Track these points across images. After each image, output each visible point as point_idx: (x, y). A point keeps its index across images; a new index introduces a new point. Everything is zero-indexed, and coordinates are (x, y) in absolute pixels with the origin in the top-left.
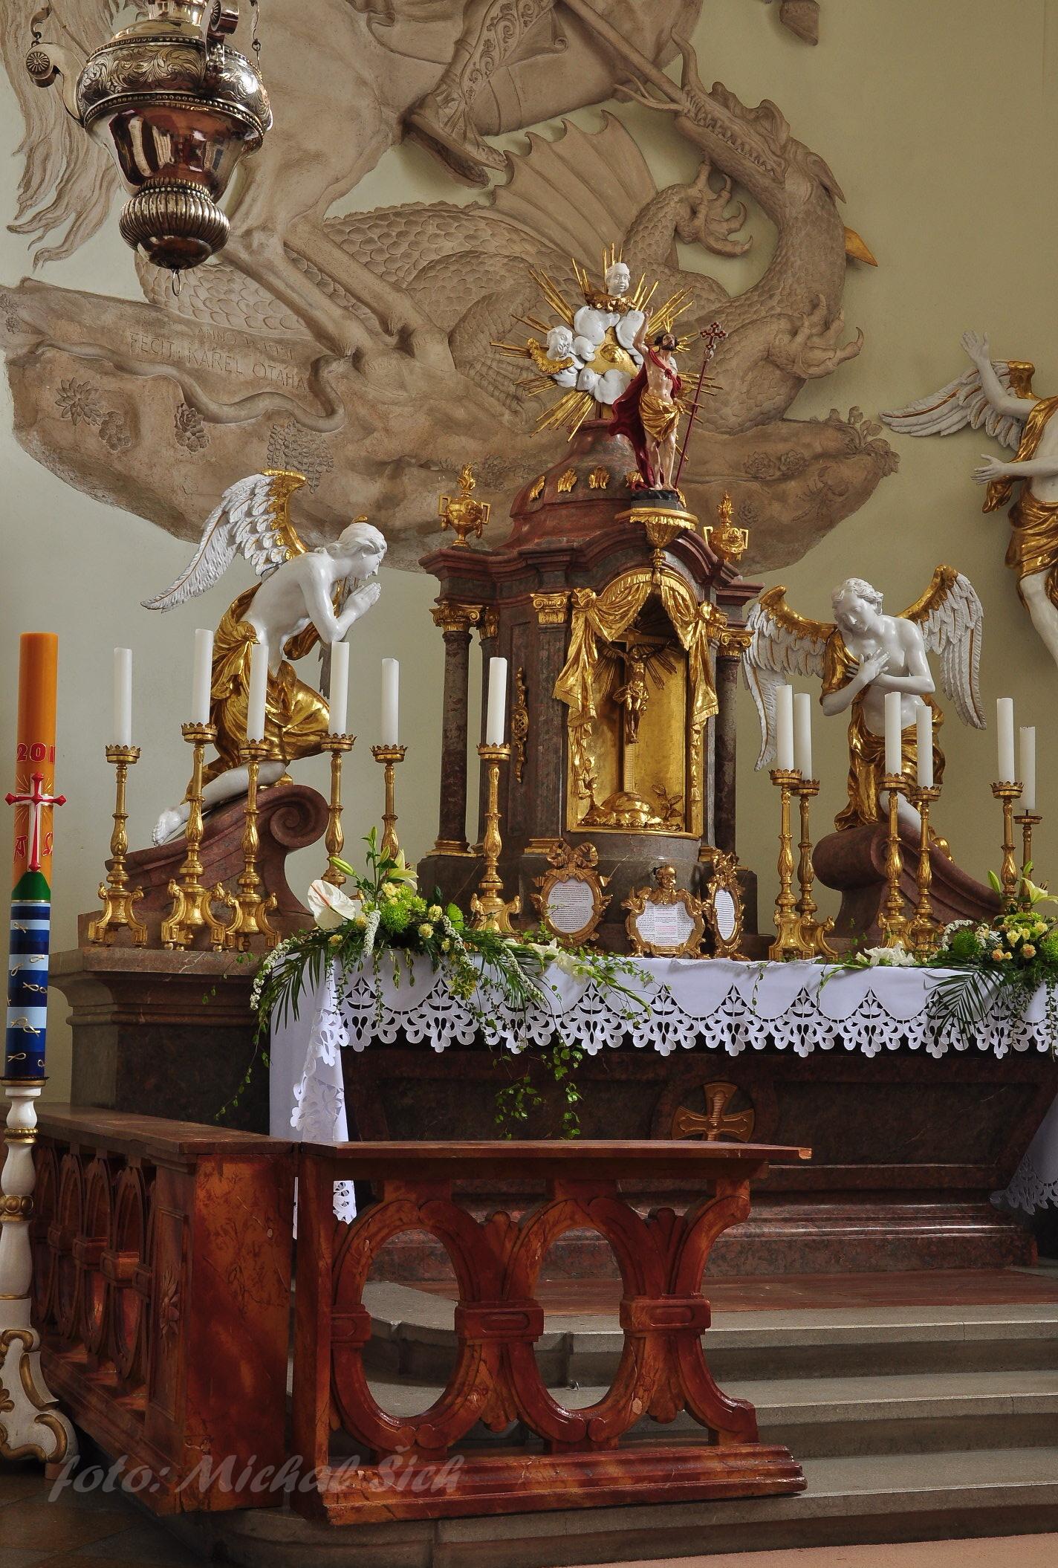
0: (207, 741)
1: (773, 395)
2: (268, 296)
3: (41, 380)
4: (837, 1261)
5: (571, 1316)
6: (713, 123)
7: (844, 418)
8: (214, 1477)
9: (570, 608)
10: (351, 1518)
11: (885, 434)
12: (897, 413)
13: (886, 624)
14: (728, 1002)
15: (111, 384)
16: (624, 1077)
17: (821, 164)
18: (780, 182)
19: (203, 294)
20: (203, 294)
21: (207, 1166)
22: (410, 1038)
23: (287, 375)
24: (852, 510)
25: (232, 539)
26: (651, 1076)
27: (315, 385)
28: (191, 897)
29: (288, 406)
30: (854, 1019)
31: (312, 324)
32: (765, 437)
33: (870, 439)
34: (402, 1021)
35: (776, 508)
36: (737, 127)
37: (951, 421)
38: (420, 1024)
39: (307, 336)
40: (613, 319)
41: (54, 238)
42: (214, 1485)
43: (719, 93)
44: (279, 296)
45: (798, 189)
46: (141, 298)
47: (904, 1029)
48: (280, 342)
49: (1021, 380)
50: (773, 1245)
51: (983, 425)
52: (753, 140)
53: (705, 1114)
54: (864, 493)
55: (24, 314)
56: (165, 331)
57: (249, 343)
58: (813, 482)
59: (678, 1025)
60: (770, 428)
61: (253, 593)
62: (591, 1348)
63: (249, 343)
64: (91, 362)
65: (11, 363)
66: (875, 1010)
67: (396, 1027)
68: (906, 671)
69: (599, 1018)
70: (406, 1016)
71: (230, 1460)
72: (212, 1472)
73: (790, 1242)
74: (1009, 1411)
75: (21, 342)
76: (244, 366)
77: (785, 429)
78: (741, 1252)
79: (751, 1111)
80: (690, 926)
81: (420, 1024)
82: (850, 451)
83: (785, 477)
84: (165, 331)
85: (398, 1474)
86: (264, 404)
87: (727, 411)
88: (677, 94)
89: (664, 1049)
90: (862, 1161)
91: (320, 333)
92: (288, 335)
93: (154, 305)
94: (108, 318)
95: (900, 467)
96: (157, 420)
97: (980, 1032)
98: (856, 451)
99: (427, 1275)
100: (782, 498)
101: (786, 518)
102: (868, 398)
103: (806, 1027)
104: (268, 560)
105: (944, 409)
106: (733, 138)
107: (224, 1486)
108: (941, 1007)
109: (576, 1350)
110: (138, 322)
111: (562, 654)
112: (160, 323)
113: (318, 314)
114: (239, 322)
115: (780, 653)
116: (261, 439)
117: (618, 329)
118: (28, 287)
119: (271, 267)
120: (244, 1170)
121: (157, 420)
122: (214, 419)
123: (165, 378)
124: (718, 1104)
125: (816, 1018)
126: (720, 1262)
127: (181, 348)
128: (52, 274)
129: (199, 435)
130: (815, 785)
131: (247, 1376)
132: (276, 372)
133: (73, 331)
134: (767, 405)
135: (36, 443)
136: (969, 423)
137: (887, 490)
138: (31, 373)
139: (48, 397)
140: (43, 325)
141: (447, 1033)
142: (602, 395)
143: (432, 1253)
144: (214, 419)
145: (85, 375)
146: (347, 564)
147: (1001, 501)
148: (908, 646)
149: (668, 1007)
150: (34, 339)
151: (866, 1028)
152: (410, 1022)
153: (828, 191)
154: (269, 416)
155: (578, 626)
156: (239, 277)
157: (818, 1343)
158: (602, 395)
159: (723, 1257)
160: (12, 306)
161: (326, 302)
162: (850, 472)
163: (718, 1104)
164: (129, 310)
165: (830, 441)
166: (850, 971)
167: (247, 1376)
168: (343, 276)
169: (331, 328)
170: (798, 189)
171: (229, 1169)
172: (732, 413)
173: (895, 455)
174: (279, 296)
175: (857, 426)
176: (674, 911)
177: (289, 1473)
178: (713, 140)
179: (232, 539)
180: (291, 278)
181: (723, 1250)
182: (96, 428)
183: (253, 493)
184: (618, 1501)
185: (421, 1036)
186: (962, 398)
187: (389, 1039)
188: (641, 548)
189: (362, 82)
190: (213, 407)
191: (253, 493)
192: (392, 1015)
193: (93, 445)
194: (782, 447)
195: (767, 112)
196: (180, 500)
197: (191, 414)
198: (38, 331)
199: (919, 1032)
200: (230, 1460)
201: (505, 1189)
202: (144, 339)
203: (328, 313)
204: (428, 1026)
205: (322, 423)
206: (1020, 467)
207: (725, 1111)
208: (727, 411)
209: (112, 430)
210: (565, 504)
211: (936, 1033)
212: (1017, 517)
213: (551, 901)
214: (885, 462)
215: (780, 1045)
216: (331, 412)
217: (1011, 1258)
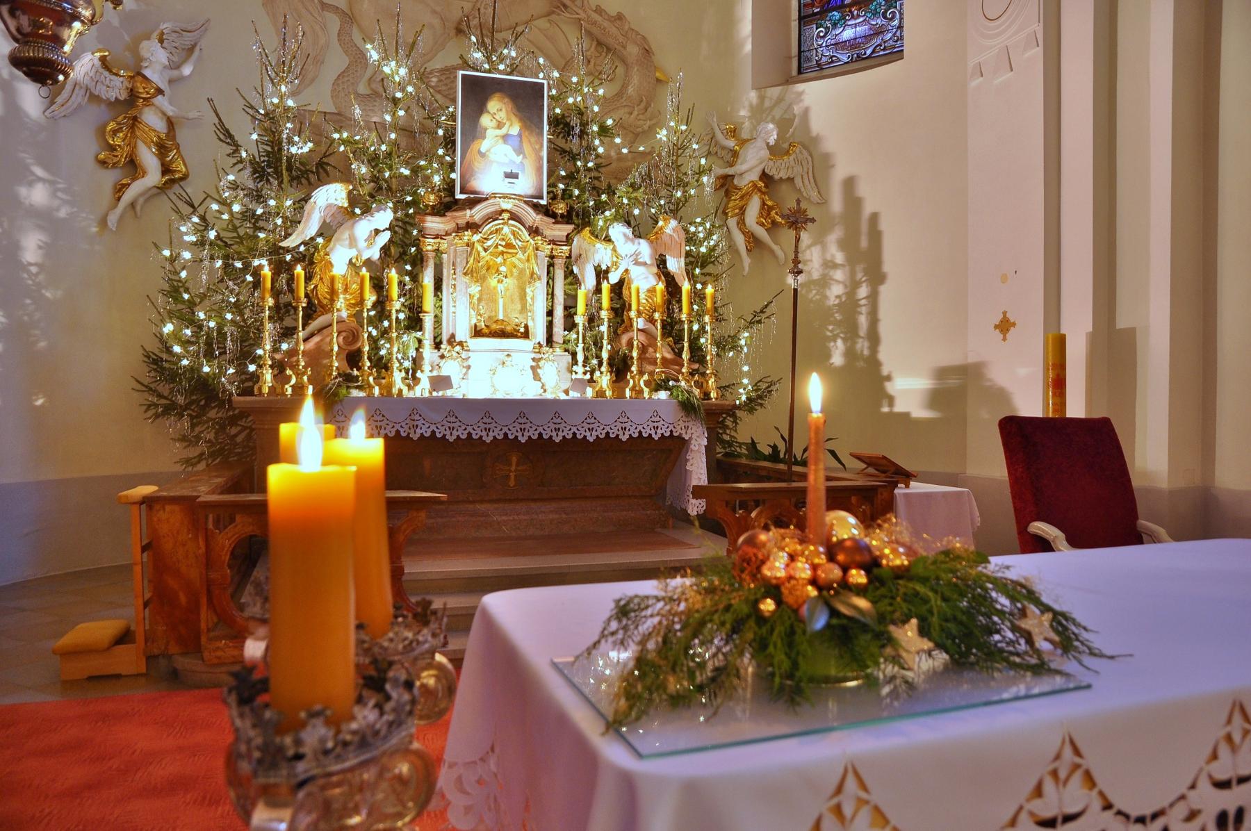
6: (595, 23)
10: (216, 661)
17: (644, 38)
18: (624, 47)
21: (157, 507)
22: (474, 437)
36: (606, 24)
38: (582, 431)
43: (599, 10)
45: (633, 50)
52: (614, 30)
66: (417, 417)
69: (527, 426)
81: (514, 430)
88: (580, 11)
106: (604, 29)
113: (164, 109)
120: (176, 508)
124: (514, 460)
131: (183, 598)
147: (722, 186)
149: (453, 419)
153: (647, 52)
167: (183, 598)
170: (633, 50)
171: (168, 508)
178: (595, 30)
187: (464, 437)
189: (434, 12)
195: (620, 17)
206: (730, 171)
207: (517, 465)
212: (728, 194)
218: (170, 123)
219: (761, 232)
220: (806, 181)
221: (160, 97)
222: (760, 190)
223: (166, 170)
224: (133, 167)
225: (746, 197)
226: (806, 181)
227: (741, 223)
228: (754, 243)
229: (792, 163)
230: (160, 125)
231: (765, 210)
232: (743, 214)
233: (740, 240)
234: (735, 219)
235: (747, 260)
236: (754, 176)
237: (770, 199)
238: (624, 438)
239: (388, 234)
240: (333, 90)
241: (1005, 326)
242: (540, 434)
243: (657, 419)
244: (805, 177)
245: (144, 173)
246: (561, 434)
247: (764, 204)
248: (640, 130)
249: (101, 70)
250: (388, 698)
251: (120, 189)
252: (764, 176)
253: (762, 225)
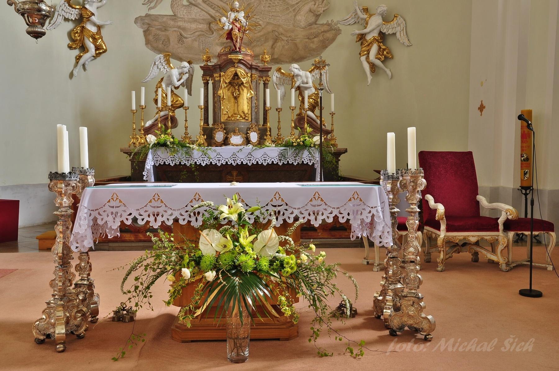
1: (312, 19)
2: (199, 10)
3: (149, 34)
9: (220, 76)
11: (339, 25)
13: (302, 73)
14: (153, 200)
15: (163, 33)
19: (185, 11)
20: (185, 11)
22: (166, 163)
23: (204, 26)
24: (331, 43)
25: (158, 68)
27: (210, 28)
28: (141, 138)
29: (203, 33)
30: (145, 209)
31: (209, 14)
32: (311, 29)
34: (165, 160)
35: (311, 45)
37: (352, 21)
39: (209, 17)
41: (152, 5)
42: (446, 349)
44: (202, 10)
46: (173, 14)
47: (273, 160)
48: (203, 19)
49: (366, 10)
54: (333, 39)
55: (146, 21)
57: (195, 21)
58: (321, 38)
59: (285, 211)
60: (312, 26)
63: (195, 21)
64: (160, 29)
65: (144, 31)
67: (333, 215)
68: (307, 83)
70: (97, 211)
71: (452, 340)
75: (146, 27)
76: (194, 26)
77: (316, 26)
80: (242, 140)
82: (331, 29)
83: (315, 37)
85: (511, 344)
86: (197, 33)
87: (301, 24)
89: (219, 165)
91: (212, 17)
92: (205, 18)
93: (175, 15)
94: (165, 19)
95: (342, 32)
96: (173, 39)
97: (182, 215)
100: (313, 42)
101: (314, 47)
102: (335, 17)
103: (279, 212)
105: (350, 19)
107: (450, 349)
108: (282, 155)
112: (176, 19)
113: (210, 13)
114: (193, 16)
115: (282, 80)
116: (196, 41)
118: (147, 16)
119: (199, 4)
121: (173, 39)
122: (186, 38)
123: (175, 31)
125: (123, 208)
127: (180, 24)
128: (152, 12)
129: (183, 41)
130: (281, 109)
132: (201, 26)
133: (157, 23)
134: (310, 22)
135: (150, 47)
137: (339, 39)
138: (147, 33)
139: (151, 38)
140: (150, 23)
141: (220, 162)
144: (186, 38)
145: (158, 32)
146: (180, 71)
148: (307, 78)
150: (148, 26)
151: (112, 213)
152: (99, 214)
154: (199, 36)
155: (222, 80)
156: (193, 7)
160: (144, 20)
161: (212, 10)
162: (329, 35)
164: (169, 17)
165: (326, 28)
166: (260, 148)
168: (216, 4)
169: (213, 15)
172: (303, 24)
174: (202, 10)
176: (239, 137)
177: (472, 345)
179: (158, 68)
180: (204, 6)
182: (161, 43)
183: (160, 58)
184: (141, 241)
185: (145, 221)
187: (162, 164)
188: (231, 63)
190: (185, 35)
191: (160, 58)
192: (370, 209)
193: (161, 46)
194: (315, 31)
196: (180, 55)
197: (181, 38)
198: (149, 24)
199: (276, 160)
200: (452, 340)
202: (172, 23)
203: (212, 12)
204: (149, 216)
205: (210, 36)
207: (237, 176)
208: (301, 24)
209: (164, 43)
211: (280, 160)
213: (216, 136)
214: (338, 32)
215: (244, 163)
216: (213, 33)
218: (99, 27)
219: (378, 62)
220: (402, 35)
221: (93, 17)
222: (377, 41)
223: (97, 48)
224: (84, 49)
225: (370, 44)
226: (402, 35)
227: (367, 58)
228: (373, 67)
229: (395, 25)
230: (93, 29)
231: (380, 51)
232: (369, 54)
233: (367, 67)
234: (365, 57)
235: (370, 77)
236: (375, 34)
237: (384, 45)
238: (219, 165)
239: (187, 75)
240: (172, 4)
241: (482, 108)
242: (242, 162)
243: (266, 156)
244: (402, 32)
245: (88, 51)
246: (266, 162)
247: (380, 48)
248: (319, 13)
249: (68, 7)
250: (297, 300)
251: (78, 58)
252: (381, 34)
253: (379, 59)
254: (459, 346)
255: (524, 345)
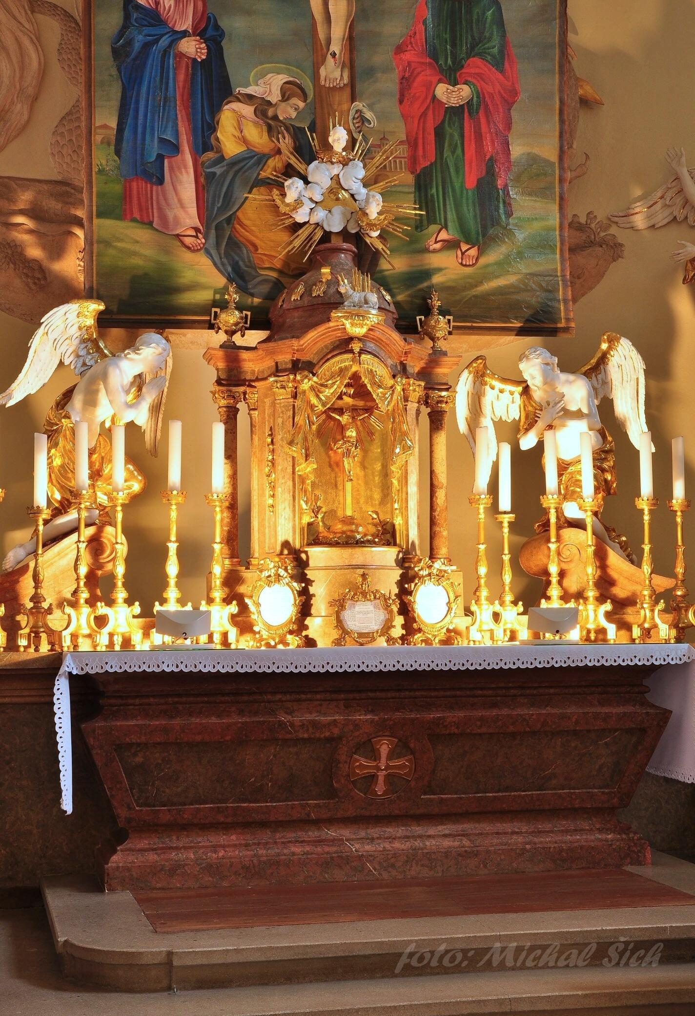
0: (569, 414)
4: (485, 866)
5: (197, 930)
7: (583, 220)
8: (502, 957)
11: (613, 230)
12: (621, 214)
16: (306, 736)
26: (327, 734)
33: (602, 234)
40: (336, 170)
50: (433, 856)
51: (686, 218)
53: (375, 760)
56: (71, 200)
61: (75, 386)
62: (189, 962)
72: (504, 958)
73: (446, 853)
74: (507, 1009)
78: (407, 862)
79: (410, 757)
84: (71, 200)
90: (506, 789)
98: (591, 244)
99: (159, 885)
104: (84, 364)
109: (175, 964)
110: (52, 195)
111: (291, 420)
117: (341, 176)
124: (384, 750)
126: (390, 869)
136: (675, 217)
142: (329, 225)
143: (162, 870)
157: (377, 952)
158: (329, 225)
159: (393, 866)
163: (384, 750)
173: (621, 245)
175: (593, 226)
181: (393, 860)
186: (668, 199)
201: (222, 819)
207: (390, 757)
210: (297, 308)
217: (629, 860)
254: (526, 957)
255: (644, 956)
